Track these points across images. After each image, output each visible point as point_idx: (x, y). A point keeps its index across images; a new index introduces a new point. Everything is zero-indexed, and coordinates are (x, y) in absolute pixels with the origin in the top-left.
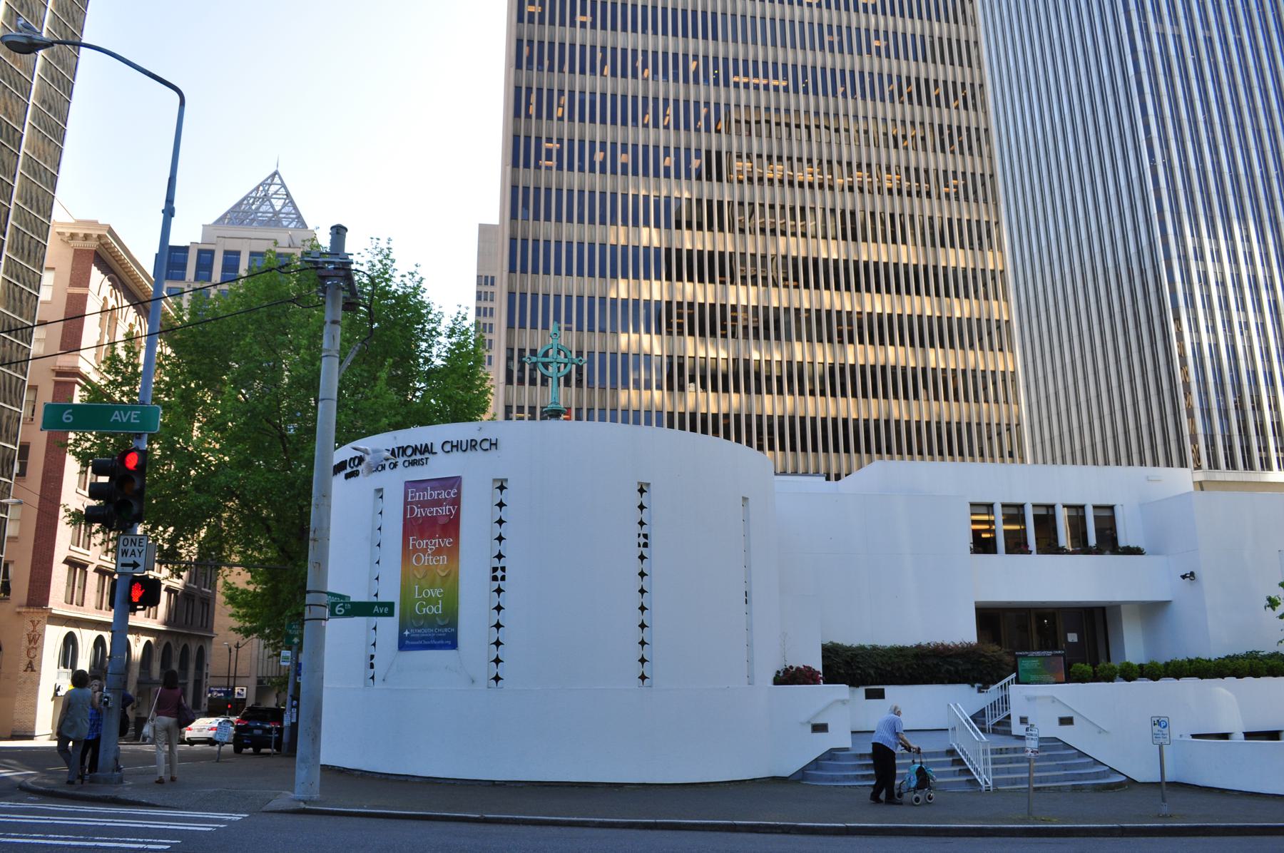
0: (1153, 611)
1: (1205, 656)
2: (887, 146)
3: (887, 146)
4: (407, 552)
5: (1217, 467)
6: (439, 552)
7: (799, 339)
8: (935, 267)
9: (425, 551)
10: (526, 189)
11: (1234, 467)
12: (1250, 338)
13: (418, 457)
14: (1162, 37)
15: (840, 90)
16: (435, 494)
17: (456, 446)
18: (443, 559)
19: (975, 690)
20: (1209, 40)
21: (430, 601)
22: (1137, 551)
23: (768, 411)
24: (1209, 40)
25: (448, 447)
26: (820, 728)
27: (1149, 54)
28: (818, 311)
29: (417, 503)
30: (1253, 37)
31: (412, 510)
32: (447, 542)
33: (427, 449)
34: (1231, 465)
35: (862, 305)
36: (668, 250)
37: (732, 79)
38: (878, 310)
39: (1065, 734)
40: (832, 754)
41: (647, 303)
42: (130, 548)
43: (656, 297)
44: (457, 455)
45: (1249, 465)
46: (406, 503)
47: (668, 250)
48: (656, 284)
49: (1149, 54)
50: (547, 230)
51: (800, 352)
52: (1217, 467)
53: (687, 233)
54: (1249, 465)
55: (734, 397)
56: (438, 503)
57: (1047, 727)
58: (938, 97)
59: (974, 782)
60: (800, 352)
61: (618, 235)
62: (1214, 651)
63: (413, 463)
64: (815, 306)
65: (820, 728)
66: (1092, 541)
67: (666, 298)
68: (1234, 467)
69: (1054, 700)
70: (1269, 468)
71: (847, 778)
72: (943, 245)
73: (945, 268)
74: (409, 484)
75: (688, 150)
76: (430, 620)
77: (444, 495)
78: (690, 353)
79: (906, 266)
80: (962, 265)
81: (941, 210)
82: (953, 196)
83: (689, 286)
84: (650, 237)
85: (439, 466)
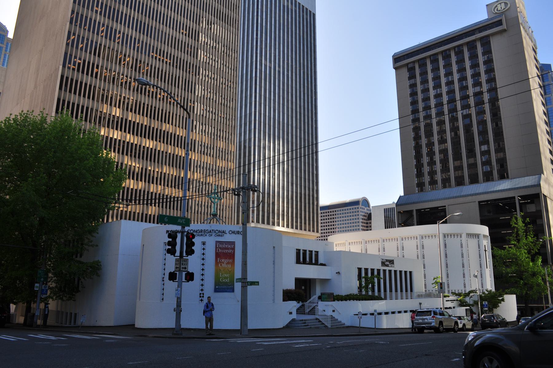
0: (325, 281)
2: (116, 63)
3: (116, 63)
4: (217, 263)
6: (228, 263)
7: (127, 154)
8: (161, 130)
9: (223, 263)
10: (67, 78)
14: (266, 66)
17: (233, 232)
18: (230, 266)
20: (279, 72)
21: (227, 278)
22: (324, 265)
24: (279, 72)
25: (231, 232)
26: (291, 313)
27: (261, 71)
28: (124, 142)
29: (220, 248)
30: (292, 75)
31: (219, 250)
35: (109, 134)
38: (115, 137)
39: (334, 314)
40: (293, 320)
42: (184, 263)
44: (233, 235)
45: (274, 224)
46: (216, 248)
48: (116, 132)
49: (261, 71)
51: (166, 169)
56: (227, 249)
57: (329, 313)
58: (138, 47)
59: (326, 326)
60: (166, 169)
62: (344, 293)
63: (219, 235)
64: (123, 139)
65: (291, 313)
66: (314, 262)
69: (332, 305)
71: (302, 326)
72: (165, 122)
73: (178, 136)
74: (217, 242)
75: (93, 64)
76: (226, 284)
77: (229, 246)
79: (138, 124)
80: (181, 135)
81: (113, 90)
82: (161, 99)
84: (117, 112)
85: (228, 238)
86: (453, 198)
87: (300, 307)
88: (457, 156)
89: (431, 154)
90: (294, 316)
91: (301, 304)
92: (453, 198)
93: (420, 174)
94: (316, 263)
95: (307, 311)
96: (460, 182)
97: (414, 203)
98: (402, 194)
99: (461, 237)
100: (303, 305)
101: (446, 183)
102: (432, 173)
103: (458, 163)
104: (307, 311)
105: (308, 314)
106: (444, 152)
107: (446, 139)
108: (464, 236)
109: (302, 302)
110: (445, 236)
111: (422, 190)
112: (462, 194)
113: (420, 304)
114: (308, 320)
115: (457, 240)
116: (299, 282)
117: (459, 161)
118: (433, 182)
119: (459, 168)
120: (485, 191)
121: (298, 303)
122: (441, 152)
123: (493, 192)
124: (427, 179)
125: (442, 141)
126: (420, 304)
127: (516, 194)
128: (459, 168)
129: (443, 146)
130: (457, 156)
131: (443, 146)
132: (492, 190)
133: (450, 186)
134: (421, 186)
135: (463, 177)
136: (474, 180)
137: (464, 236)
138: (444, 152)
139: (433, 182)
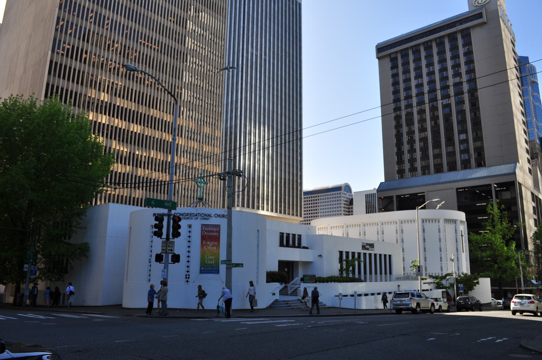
0: (307, 264)
1: (322, 276)
4: (202, 245)
5: (244, 207)
9: (209, 245)
10: (56, 63)
11: (249, 207)
12: (260, 164)
13: (206, 217)
14: (252, 54)
15: (176, 57)
16: (212, 229)
18: (215, 248)
19: (7, 98)
20: (265, 60)
21: (212, 260)
22: (307, 248)
23: (139, 174)
24: (265, 60)
25: (216, 216)
26: (274, 294)
31: (204, 233)
32: (216, 243)
33: (209, 215)
34: (248, 207)
36: (110, 104)
37: (139, 40)
41: (100, 123)
42: (170, 245)
43: (104, 122)
44: (219, 218)
46: (202, 231)
47: (110, 104)
48: (104, 117)
50: (62, 83)
51: (153, 154)
52: (244, 207)
53: (118, 99)
54: (253, 207)
55: (128, 167)
60: (153, 154)
61: (92, 93)
63: (205, 219)
65: (274, 294)
67: (107, 123)
68: (249, 207)
70: (259, 209)
76: (211, 265)
77: (215, 229)
78: (114, 147)
83: (116, 120)
84: (104, 97)
86: (434, 184)
87: (283, 288)
88: (437, 144)
89: (411, 142)
90: (277, 297)
91: (284, 285)
92: (434, 184)
93: (400, 161)
94: (299, 246)
95: (290, 292)
96: (439, 169)
97: (394, 189)
98: (383, 181)
99: (439, 222)
100: (286, 287)
101: (425, 170)
102: (412, 161)
103: (437, 151)
104: (290, 292)
105: (291, 295)
106: (424, 140)
107: (426, 128)
108: (442, 221)
109: (285, 283)
110: (423, 222)
111: (402, 177)
112: (441, 181)
113: (399, 286)
114: (291, 301)
115: (435, 226)
116: (282, 264)
117: (438, 150)
118: (413, 169)
119: (438, 156)
120: (462, 178)
121: (281, 284)
122: (421, 140)
123: (471, 179)
124: (407, 166)
125: (423, 129)
126: (399, 286)
127: (493, 183)
128: (438, 156)
129: (423, 135)
130: (437, 144)
131: (423, 135)
132: (470, 177)
133: (429, 173)
134: (401, 172)
135: (441, 165)
136: (452, 167)
137: (442, 221)
138: (424, 140)
139: (413, 169)
